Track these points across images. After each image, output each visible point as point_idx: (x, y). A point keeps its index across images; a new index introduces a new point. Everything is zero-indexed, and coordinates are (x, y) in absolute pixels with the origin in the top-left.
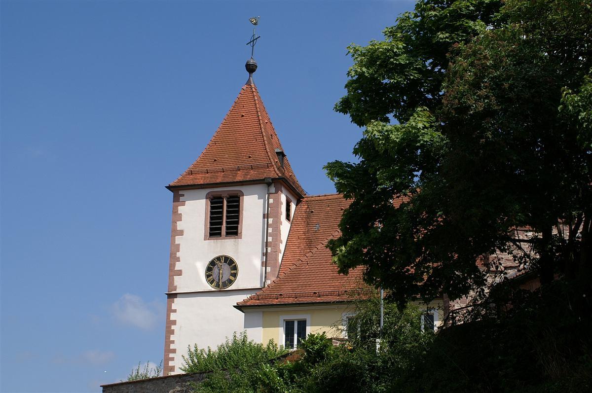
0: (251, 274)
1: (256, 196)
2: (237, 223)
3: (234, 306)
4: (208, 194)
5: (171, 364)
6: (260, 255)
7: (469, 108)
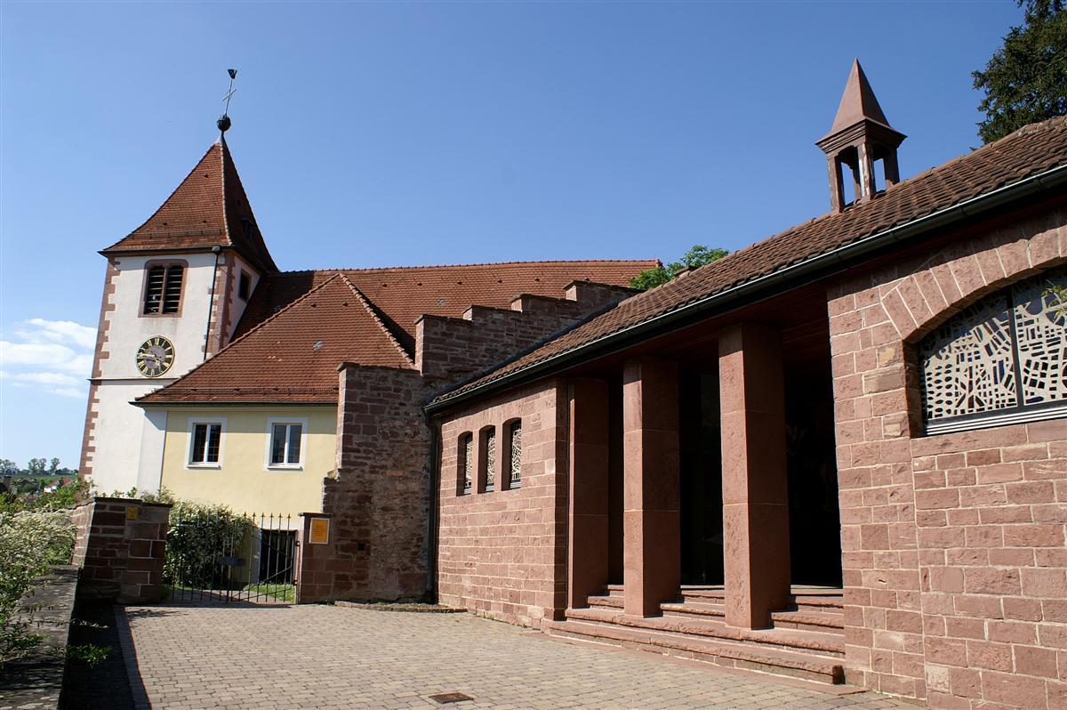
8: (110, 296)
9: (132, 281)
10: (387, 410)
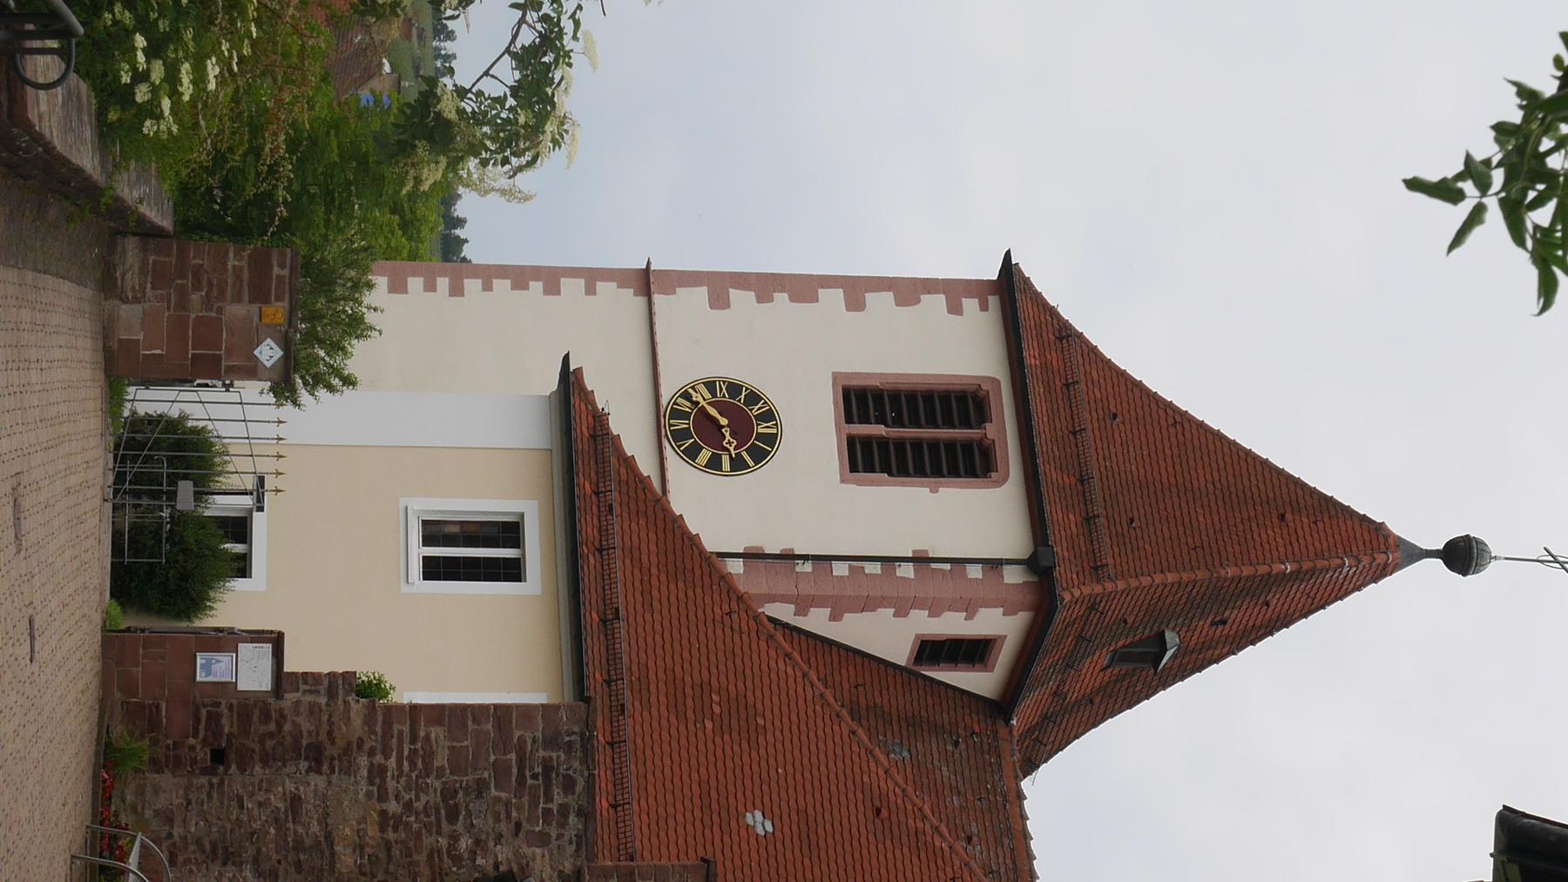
0: (716, 509)
3: (1008, 253)
8: (889, 296)
9: (964, 351)
10: (503, 795)
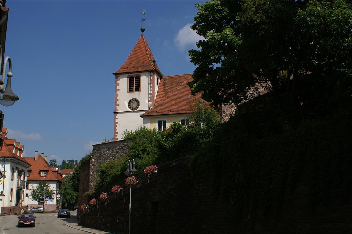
0: (145, 105)
1: (146, 76)
2: (139, 86)
3: (140, 116)
4: (128, 76)
5: (116, 137)
6: (148, 98)
7: (253, 21)
